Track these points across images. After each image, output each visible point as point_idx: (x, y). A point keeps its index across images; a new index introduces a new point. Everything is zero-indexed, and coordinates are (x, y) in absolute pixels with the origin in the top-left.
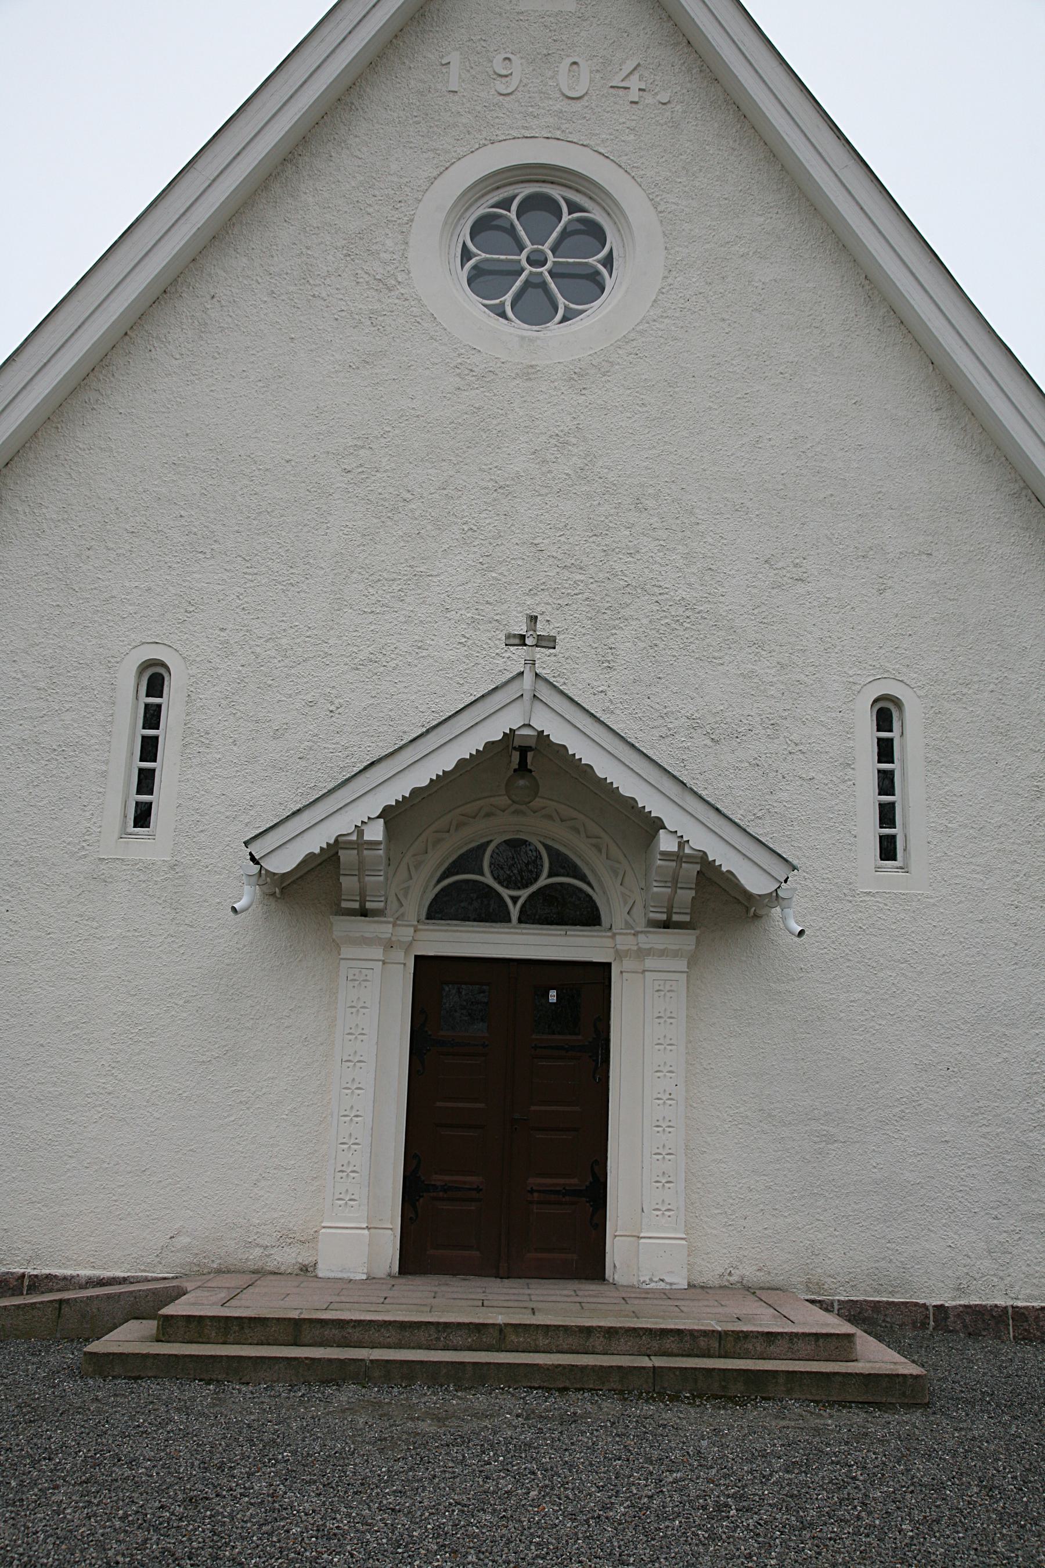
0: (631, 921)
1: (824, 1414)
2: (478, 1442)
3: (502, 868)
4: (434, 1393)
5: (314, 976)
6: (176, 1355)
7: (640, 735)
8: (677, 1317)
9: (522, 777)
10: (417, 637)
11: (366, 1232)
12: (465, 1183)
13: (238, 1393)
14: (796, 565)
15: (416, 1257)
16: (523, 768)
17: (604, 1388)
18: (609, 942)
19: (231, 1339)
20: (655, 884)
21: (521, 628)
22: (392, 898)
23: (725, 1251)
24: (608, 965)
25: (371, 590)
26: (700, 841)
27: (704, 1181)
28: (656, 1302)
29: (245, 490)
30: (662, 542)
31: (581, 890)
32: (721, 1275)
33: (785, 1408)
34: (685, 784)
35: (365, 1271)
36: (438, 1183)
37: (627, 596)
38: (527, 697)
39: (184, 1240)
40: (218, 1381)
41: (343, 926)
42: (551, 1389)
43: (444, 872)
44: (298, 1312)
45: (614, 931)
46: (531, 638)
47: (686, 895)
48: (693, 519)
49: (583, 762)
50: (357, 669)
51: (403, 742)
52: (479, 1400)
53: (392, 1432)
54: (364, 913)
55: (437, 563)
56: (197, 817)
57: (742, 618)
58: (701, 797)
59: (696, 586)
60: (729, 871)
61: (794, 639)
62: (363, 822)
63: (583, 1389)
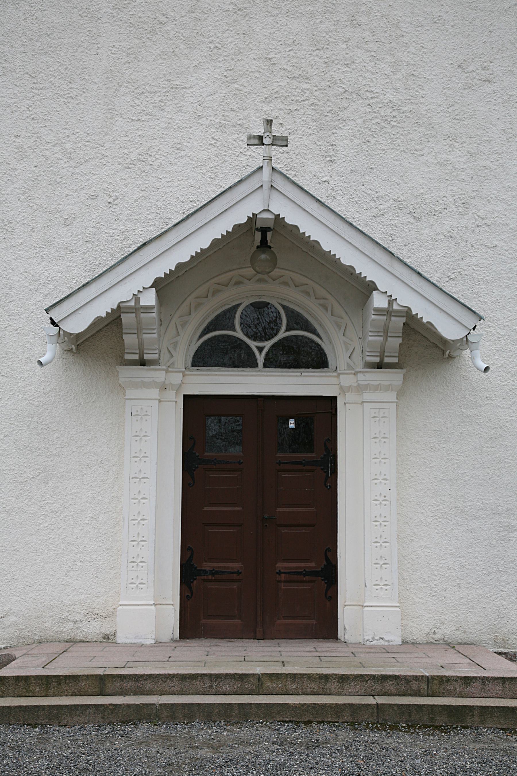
0: (352, 364)
1: (511, 739)
2: (243, 763)
3: (250, 327)
4: (209, 728)
5: (105, 413)
6: (8, 707)
7: (357, 215)
8: (394, 666)
9: (264, 252)
10: (175, 140)
11: (153, 607)
12: (228, 568)
13: (58, 734)
14: (484, 68)
15: (194, 623)
16: (264, 245)
17: (340, 721)
18: (335, 381)
19: (51, 692)
20: (370, 334)
21: (260, 131)
22: (164, 351)
23: (430, 615)
24: (334, 399)
25: (137, 101)
26: (405, 299)
27: (412, 562)
28: (377, 655)
29: (27, 15)
30: (373, 54)
31: (312, 341)
32: (428, 634)
33: (480, 734)
34: (393, 254)
35: (154, 637)
36: (208, 569)
37: (344, 100)
38: (266, 187)
39: (12, 619)
40: (42, 725)
41: (128, 374)
42: (298, 722)
43: (205, 329)
44: (103, 670)
45: (339, 372)
46: (268, 139)
47: (394, 343)
48: (399, 32)
49: (312, 239)
50: (129, 168)
51: (168, 227)
52: (244, 732)
53: (177, 758)
54: (143, 363)
55: (189, 77)
56: (6, 290)
57: (439, 115)
58: (406, 264)
59: (401, 90)
60: (428, 322)
61: (482, 132)
62: (139, 291)
63: (323, 722)
